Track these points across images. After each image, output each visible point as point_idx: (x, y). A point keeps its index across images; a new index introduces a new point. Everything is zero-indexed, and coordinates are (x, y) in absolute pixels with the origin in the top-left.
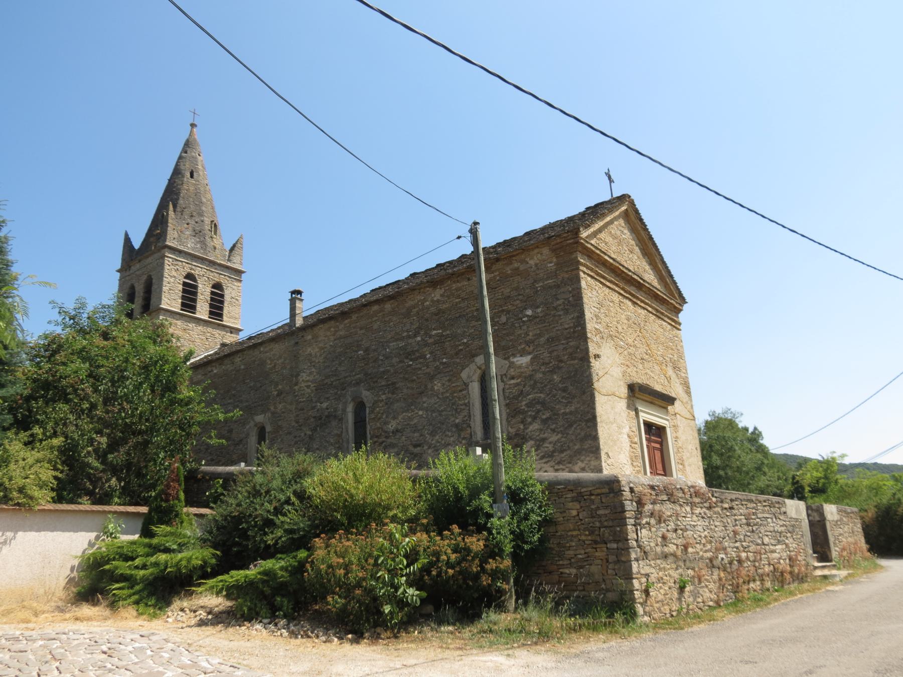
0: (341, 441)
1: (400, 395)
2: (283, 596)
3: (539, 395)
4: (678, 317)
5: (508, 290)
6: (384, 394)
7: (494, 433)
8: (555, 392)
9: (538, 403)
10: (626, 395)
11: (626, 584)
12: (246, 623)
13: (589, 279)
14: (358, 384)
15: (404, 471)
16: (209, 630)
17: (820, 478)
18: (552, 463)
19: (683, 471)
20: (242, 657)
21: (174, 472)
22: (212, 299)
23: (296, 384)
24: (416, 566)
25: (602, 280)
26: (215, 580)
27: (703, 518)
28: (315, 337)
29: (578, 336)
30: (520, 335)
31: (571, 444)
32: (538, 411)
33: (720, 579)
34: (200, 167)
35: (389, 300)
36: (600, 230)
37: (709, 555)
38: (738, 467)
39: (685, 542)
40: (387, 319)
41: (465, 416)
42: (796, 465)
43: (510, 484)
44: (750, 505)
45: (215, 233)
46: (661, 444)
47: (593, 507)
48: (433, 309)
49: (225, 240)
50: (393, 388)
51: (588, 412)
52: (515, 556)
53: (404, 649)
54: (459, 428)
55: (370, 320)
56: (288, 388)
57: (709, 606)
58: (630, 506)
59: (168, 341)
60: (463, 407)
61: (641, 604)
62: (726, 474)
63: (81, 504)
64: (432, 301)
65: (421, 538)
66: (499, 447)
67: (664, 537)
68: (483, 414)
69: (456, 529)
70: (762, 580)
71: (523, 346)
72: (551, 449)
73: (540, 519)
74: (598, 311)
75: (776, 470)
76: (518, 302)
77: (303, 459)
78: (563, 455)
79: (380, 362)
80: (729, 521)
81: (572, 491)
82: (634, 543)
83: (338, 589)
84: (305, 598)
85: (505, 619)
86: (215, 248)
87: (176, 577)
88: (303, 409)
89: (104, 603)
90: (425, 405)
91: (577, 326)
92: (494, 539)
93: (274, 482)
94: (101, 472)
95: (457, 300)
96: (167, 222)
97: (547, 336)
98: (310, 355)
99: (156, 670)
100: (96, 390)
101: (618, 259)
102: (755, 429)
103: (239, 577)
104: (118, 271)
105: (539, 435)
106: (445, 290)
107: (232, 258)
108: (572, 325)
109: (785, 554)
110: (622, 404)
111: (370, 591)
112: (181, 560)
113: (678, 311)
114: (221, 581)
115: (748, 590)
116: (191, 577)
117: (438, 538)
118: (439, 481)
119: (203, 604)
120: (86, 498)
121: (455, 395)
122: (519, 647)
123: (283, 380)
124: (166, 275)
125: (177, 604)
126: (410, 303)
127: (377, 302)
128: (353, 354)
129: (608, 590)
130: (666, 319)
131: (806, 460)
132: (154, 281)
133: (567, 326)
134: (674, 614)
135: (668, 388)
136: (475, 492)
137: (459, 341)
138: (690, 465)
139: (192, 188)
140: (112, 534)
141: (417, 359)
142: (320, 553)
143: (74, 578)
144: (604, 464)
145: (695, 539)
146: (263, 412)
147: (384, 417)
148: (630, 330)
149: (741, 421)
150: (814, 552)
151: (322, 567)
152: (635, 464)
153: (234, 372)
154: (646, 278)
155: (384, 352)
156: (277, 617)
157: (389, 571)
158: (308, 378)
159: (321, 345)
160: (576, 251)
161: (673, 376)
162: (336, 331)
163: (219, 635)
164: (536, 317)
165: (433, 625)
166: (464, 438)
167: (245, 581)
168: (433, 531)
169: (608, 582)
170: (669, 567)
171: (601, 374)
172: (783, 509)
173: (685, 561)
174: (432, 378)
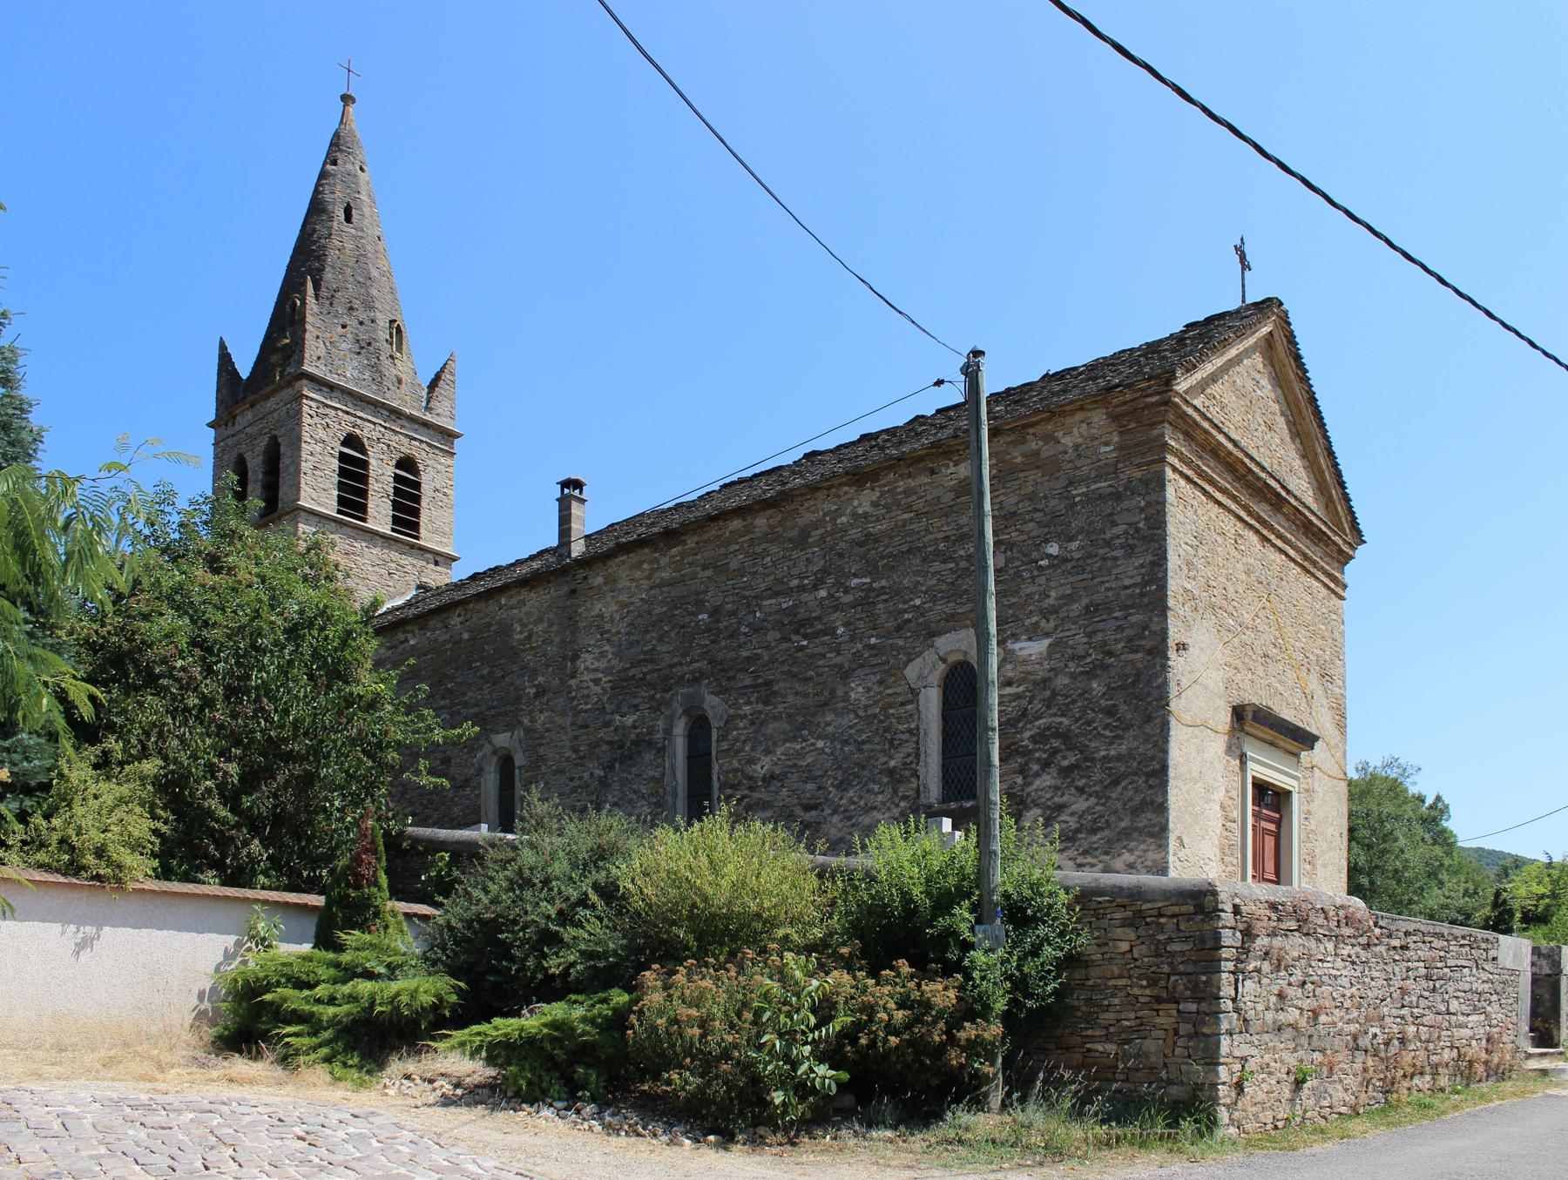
0: (661, 790)
1: (780, 708)
2: (587, 1066)
3: (1059, 719)
4: (1343, 573)
5: (1014, 499)
6: (750, 703)
7: (987, 793)
8: (1091, 715)
9: (1056, 735)
10: (1227, 727)
11: (1206, 1073)
12: (524, 1105)
13: (1182, 482)
14: (696, 680)
15: (800, 857)
16: (462, 1114)
17: (1543, 896)
18: (1072, 853)
19: (1312, 875)
20: (531, 1160)
21: (366, 836)
22: (397, 491)
23: (573, 676)
24: (835, 1026)
25: (1207, 487)
26: (466, 1031)
27: (1353, 963)
28: (611, 581)
29: (1150, 603)
30: (1030, 596)
31: (1113, 819)
32: (1055, 751)
33: (1365, 1070)
34: (364, 197)
35: (766, 509)
36: (1213, 378)
37: (1354, 1027)
38: (1396, 871)
39: (1316, 1004)
40: (758, 549)
41: (909, 755)
42: (1496, 869)
43: (1011, 890)
44: (1437, 943)
45: (399, 349)
46: (1278, 823)
47: (1161, 937)
48: (854, 533)
49: (417, 365)
50: (765, 690)
51: (1152, 758)
52: (1007, 1018)
53: (816, 1164)
54: (894, 778)
55: (723, 551)
56: (557, 681)
57: (1340, 1114)
58: (1229, 938)
59: (329, 578)
60: (905, 737)
61: (1227, 1106)
62: (1372, 883)
63: (204, 883)
64: (854, 515)
65: (839, 979)
66: (994, 820)
67: (1281, 996)
68: (944, 752)
69: (905, 967)
70: (1435, 1074)
71: (1034, 619)
72: (1073, 825)
73: (1060, 954)
74: (1193, 552)
75: (1463, 879)
76: (1031, 525)
77: (610, 824)
78: (1094, 838)
79: (742, 639)
80: (1397, 969)
81: (1124, 906)
82: (1229, 1003)
83: (688, 1060)
84: (627, 1070)
85: (985, 1123)
86: (400, 381)
87: (391, 1021)
88: (587, 727)
89: (270, 1056)
90: (830, 729)
91: (1148, 583)
92: (974, 987)
93: (556, 864)
94: (233, 828)
95: (906, 516)
96: (303, 321)
97: (1085, 601)
98: (601, 616)
99: (395, 1172)
100: (209, 671)
101: (1243, 444)
102: (1438, 798)
103: (509, 1030)
104: (210, 425)
105: (1052, 797)
106: (882, 494)
107: (433, 404)
108: (1139, 579)
109: (1482, 1031)
110: (1218, 745)
111: (747, 1067)
112: (398, 994)
113: (1344, 559)
114: (479, 1034)
115: (1409, 1089)
116: (416, 1023)
117: (871, 982)
118: (873, 879)
119: (443, 1070)
120: (211, 873)
121: (891, 711)
122: (1011, 1169)
123: (547, 666)
124: (306, 437)
125: (396, 1066)
126: (807, 518)
127: (739, 512)
128: (687, 619)
129: (1170, 1082)
130: (1319, 574)
131: (1518, 863)
132: (282, 449)
133: (1127, 582)
134: (1280, 1124)
135: (1305, 716)
136: (944, 902)
137: (905, 602)
138: (1324, 866)
139: (349, 246)
140: (264, 939)
141: (817, 634)
142: (655, 998)
143: (206, 1011)
144: (1171, 858)
145: (1334, 999)
146: (510, 727)
147: (747, 748)
148: (1250, 596)
149: (1415, 783)
150: (1531, 1030)
151: (659, 1021)
152: (1227, 859)
153: (449, 646)
154: (1291, 487)
155: (750, 618)
156: (580, 1099)
157: (781, 1035)
158: (596, 664)
159: (623, 597)
160: (1163, 422)
161: (1319, 692)
162: (653, 571)
163: (480, 1123)
164: (1067, 560)
165: (857, 1127)
166: (904, 798)
167: (520, 1036)
168: (860, 969)
169: (1172, 1068)
170: (1282, 1046)
171: (1185, 682)
172: (1492, 953)
173: (1310, 1037)
174: (845, 675)
